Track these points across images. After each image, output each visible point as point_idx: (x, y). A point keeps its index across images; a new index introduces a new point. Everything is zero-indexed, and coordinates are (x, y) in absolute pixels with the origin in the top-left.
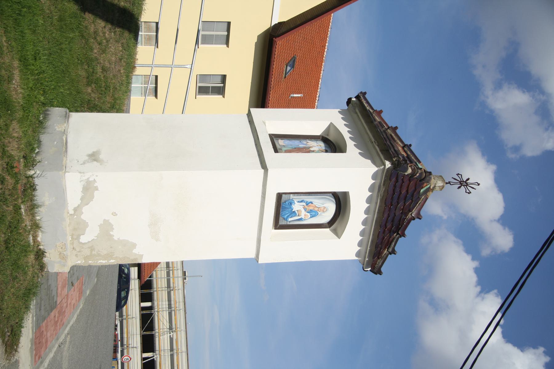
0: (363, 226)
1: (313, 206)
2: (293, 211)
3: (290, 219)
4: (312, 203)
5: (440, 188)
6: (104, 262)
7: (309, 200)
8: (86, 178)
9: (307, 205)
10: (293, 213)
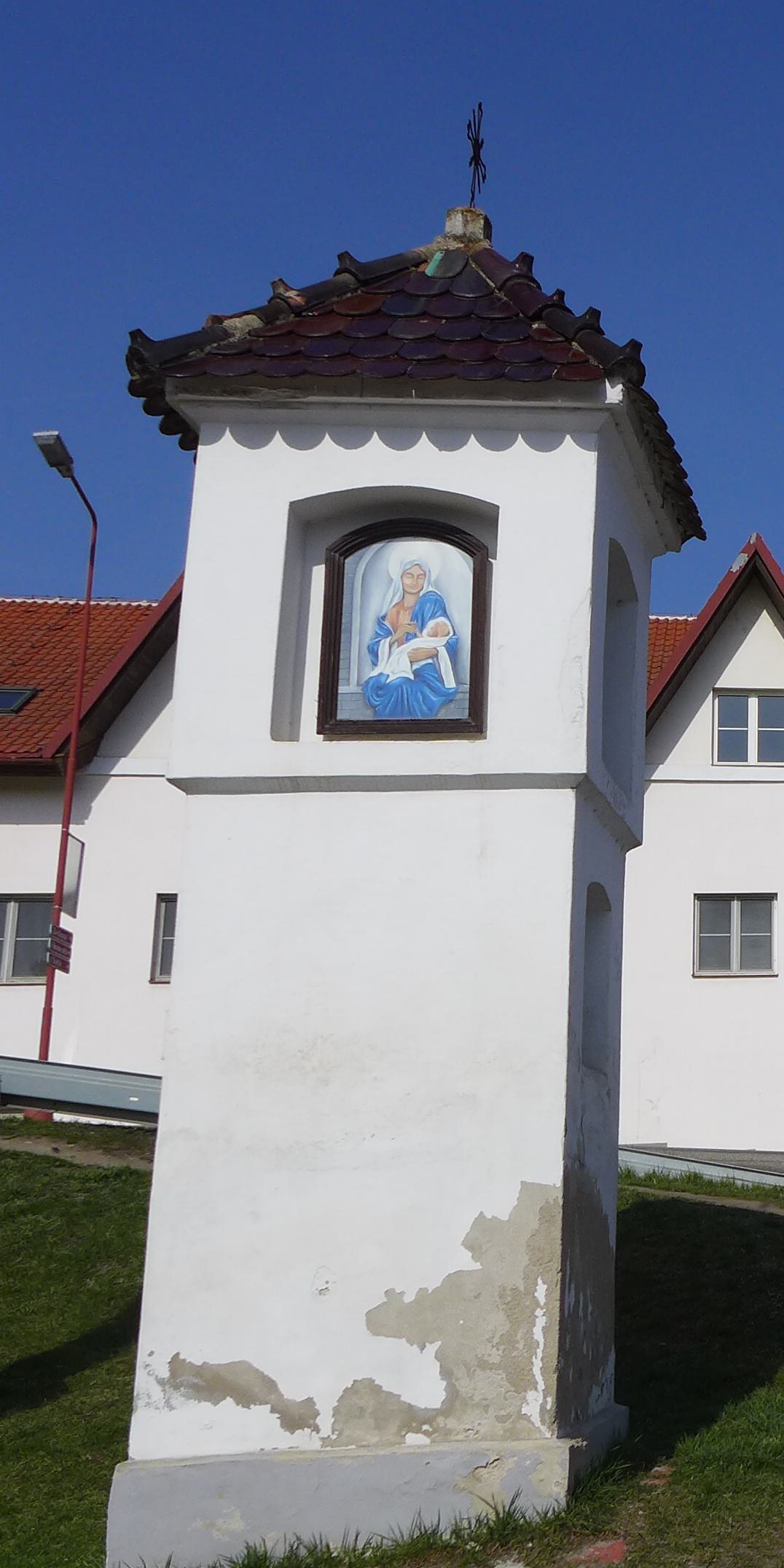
0: (421, 437)
1: (398, 613)
2: (412, 677)
3: (450, 682)
4: (384, 618)
5: (473, 221)
6: (541, 1322)
7: (370, 626)
8: (159, 1388)
9: (389, 633)
10: (425, 675)
